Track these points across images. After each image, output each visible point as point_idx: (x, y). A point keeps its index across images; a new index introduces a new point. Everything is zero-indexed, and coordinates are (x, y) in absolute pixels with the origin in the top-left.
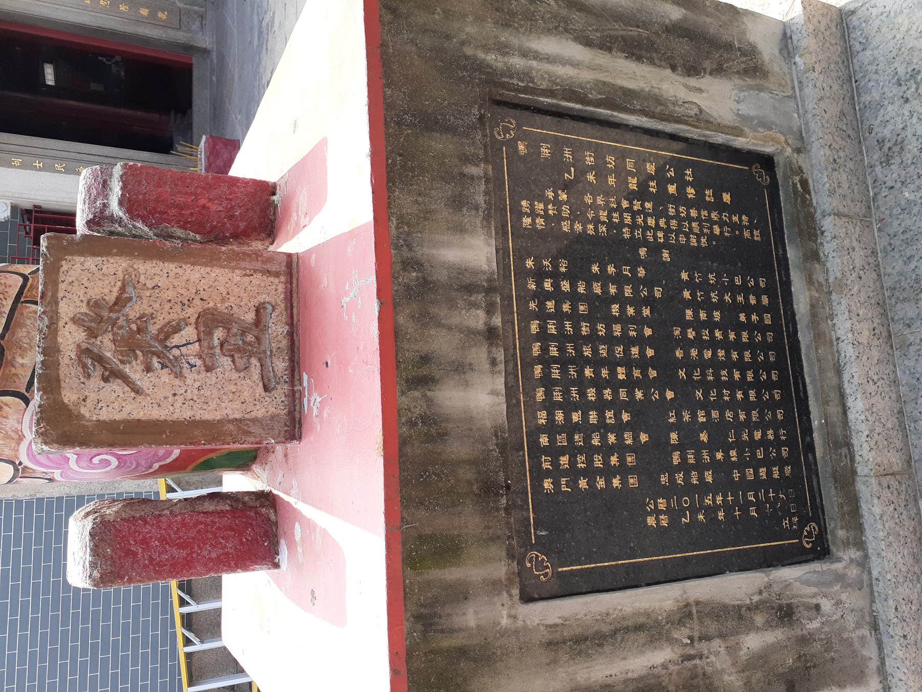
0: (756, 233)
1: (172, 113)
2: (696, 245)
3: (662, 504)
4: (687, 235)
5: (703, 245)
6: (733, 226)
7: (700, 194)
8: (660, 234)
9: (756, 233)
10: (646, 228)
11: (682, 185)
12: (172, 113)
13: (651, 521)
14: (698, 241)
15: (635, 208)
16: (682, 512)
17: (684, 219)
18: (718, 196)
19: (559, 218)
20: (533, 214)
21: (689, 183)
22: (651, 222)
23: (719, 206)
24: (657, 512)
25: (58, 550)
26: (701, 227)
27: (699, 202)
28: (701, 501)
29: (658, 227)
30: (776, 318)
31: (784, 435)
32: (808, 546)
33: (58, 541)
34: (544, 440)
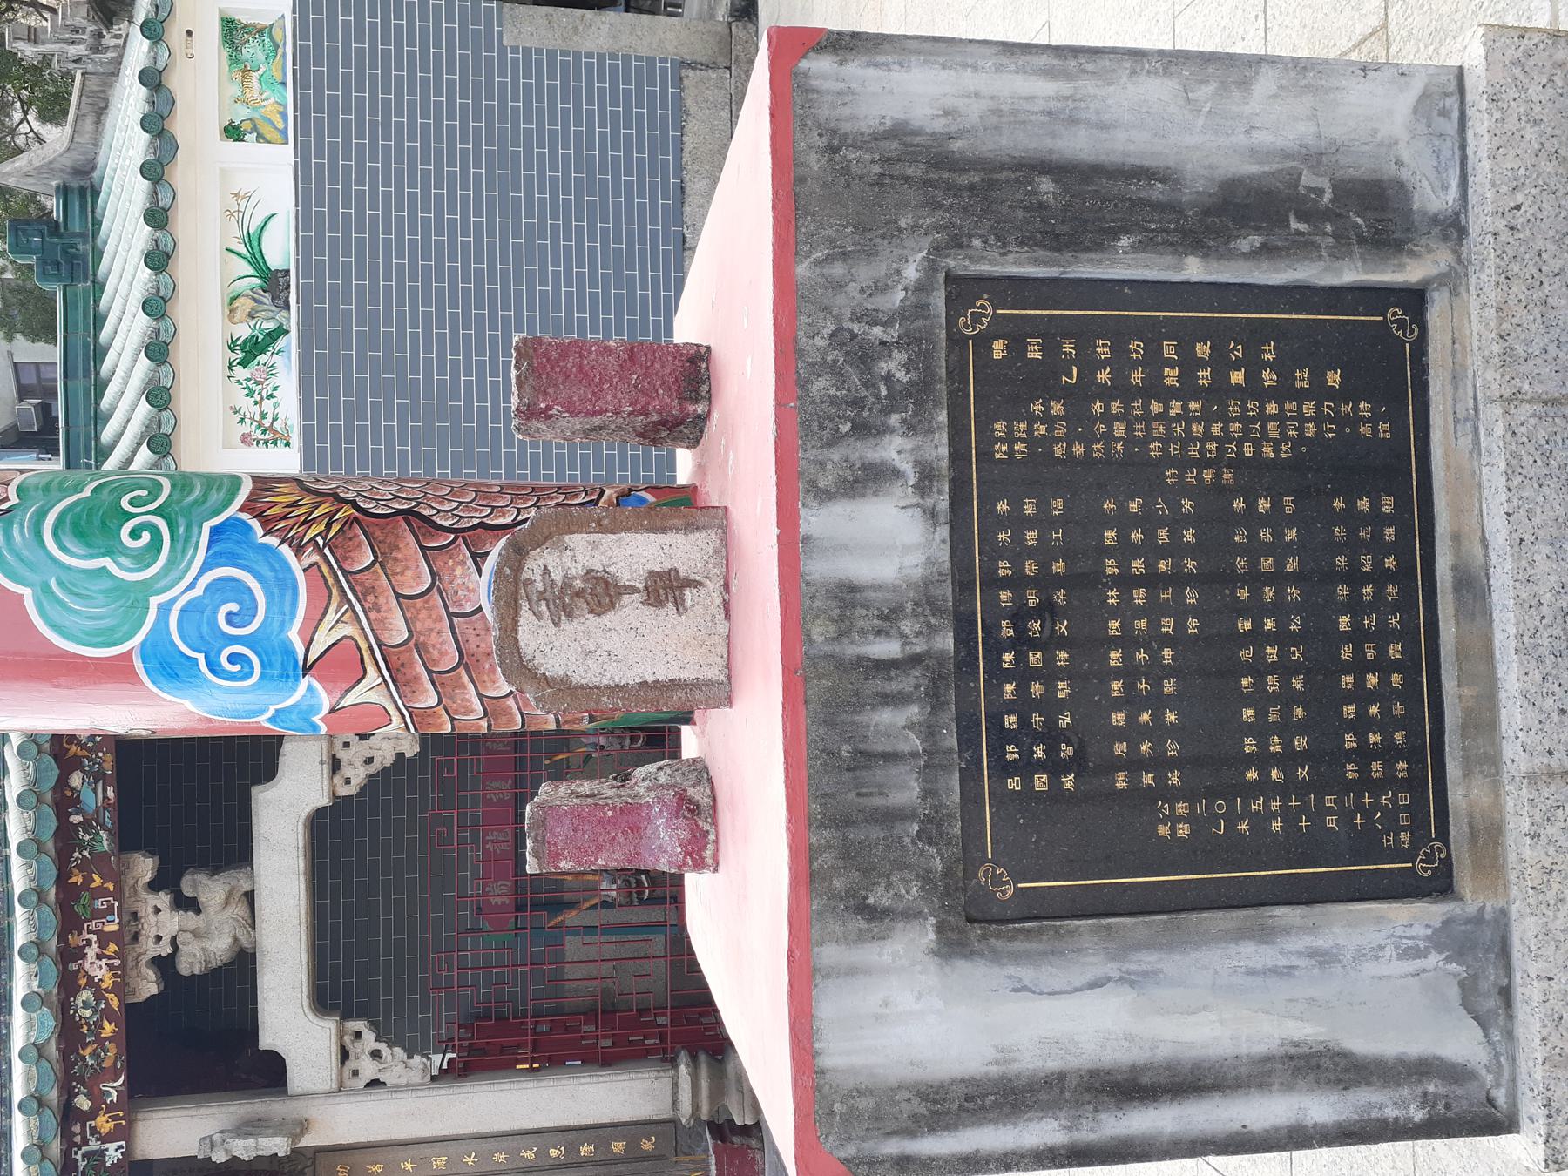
0: (1384, 427)
1: (683, 1057)
2: (1272, 455)
3: (1182, 808)
4: (1257, 443)
5: (1284, 455)
6: (1340, 420)
7: (1285, 376)
8: (1211, 446)
9: (1384, 427)
10: (1189, 439)
11: (1253, 367)
12: (683, 1057)
13: (1163, 830)
14: (1276, 450)
15: (1172, 413)
16: (1214, 819)
17: (1253, 420)
18: (1317, 377)
19: (1049, 440)
20: (1010, 439)
21: (1267, 365)
22: (1196, 429)
23: (1319, 391)
24: (1174, 820)
25: (306, 179)
26: (1283, 428)
27: (1285, 391)
28: (1245, 805)
29: (1208, 436)
30: (1405, 531)
31: (1331, 430)
32: (1425, 875)
33: (306, 192)
34: (1011, 721)
